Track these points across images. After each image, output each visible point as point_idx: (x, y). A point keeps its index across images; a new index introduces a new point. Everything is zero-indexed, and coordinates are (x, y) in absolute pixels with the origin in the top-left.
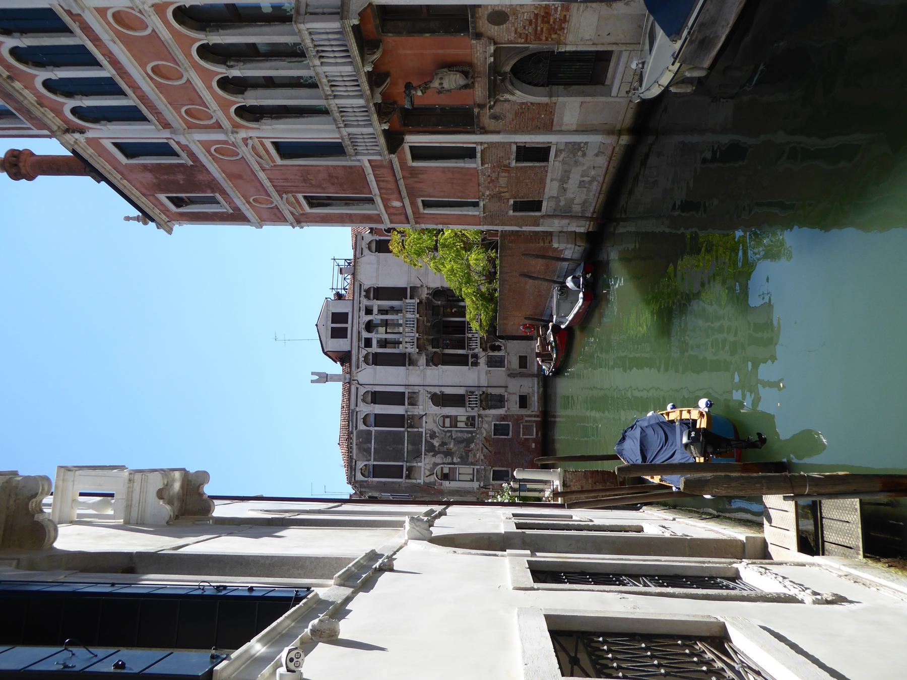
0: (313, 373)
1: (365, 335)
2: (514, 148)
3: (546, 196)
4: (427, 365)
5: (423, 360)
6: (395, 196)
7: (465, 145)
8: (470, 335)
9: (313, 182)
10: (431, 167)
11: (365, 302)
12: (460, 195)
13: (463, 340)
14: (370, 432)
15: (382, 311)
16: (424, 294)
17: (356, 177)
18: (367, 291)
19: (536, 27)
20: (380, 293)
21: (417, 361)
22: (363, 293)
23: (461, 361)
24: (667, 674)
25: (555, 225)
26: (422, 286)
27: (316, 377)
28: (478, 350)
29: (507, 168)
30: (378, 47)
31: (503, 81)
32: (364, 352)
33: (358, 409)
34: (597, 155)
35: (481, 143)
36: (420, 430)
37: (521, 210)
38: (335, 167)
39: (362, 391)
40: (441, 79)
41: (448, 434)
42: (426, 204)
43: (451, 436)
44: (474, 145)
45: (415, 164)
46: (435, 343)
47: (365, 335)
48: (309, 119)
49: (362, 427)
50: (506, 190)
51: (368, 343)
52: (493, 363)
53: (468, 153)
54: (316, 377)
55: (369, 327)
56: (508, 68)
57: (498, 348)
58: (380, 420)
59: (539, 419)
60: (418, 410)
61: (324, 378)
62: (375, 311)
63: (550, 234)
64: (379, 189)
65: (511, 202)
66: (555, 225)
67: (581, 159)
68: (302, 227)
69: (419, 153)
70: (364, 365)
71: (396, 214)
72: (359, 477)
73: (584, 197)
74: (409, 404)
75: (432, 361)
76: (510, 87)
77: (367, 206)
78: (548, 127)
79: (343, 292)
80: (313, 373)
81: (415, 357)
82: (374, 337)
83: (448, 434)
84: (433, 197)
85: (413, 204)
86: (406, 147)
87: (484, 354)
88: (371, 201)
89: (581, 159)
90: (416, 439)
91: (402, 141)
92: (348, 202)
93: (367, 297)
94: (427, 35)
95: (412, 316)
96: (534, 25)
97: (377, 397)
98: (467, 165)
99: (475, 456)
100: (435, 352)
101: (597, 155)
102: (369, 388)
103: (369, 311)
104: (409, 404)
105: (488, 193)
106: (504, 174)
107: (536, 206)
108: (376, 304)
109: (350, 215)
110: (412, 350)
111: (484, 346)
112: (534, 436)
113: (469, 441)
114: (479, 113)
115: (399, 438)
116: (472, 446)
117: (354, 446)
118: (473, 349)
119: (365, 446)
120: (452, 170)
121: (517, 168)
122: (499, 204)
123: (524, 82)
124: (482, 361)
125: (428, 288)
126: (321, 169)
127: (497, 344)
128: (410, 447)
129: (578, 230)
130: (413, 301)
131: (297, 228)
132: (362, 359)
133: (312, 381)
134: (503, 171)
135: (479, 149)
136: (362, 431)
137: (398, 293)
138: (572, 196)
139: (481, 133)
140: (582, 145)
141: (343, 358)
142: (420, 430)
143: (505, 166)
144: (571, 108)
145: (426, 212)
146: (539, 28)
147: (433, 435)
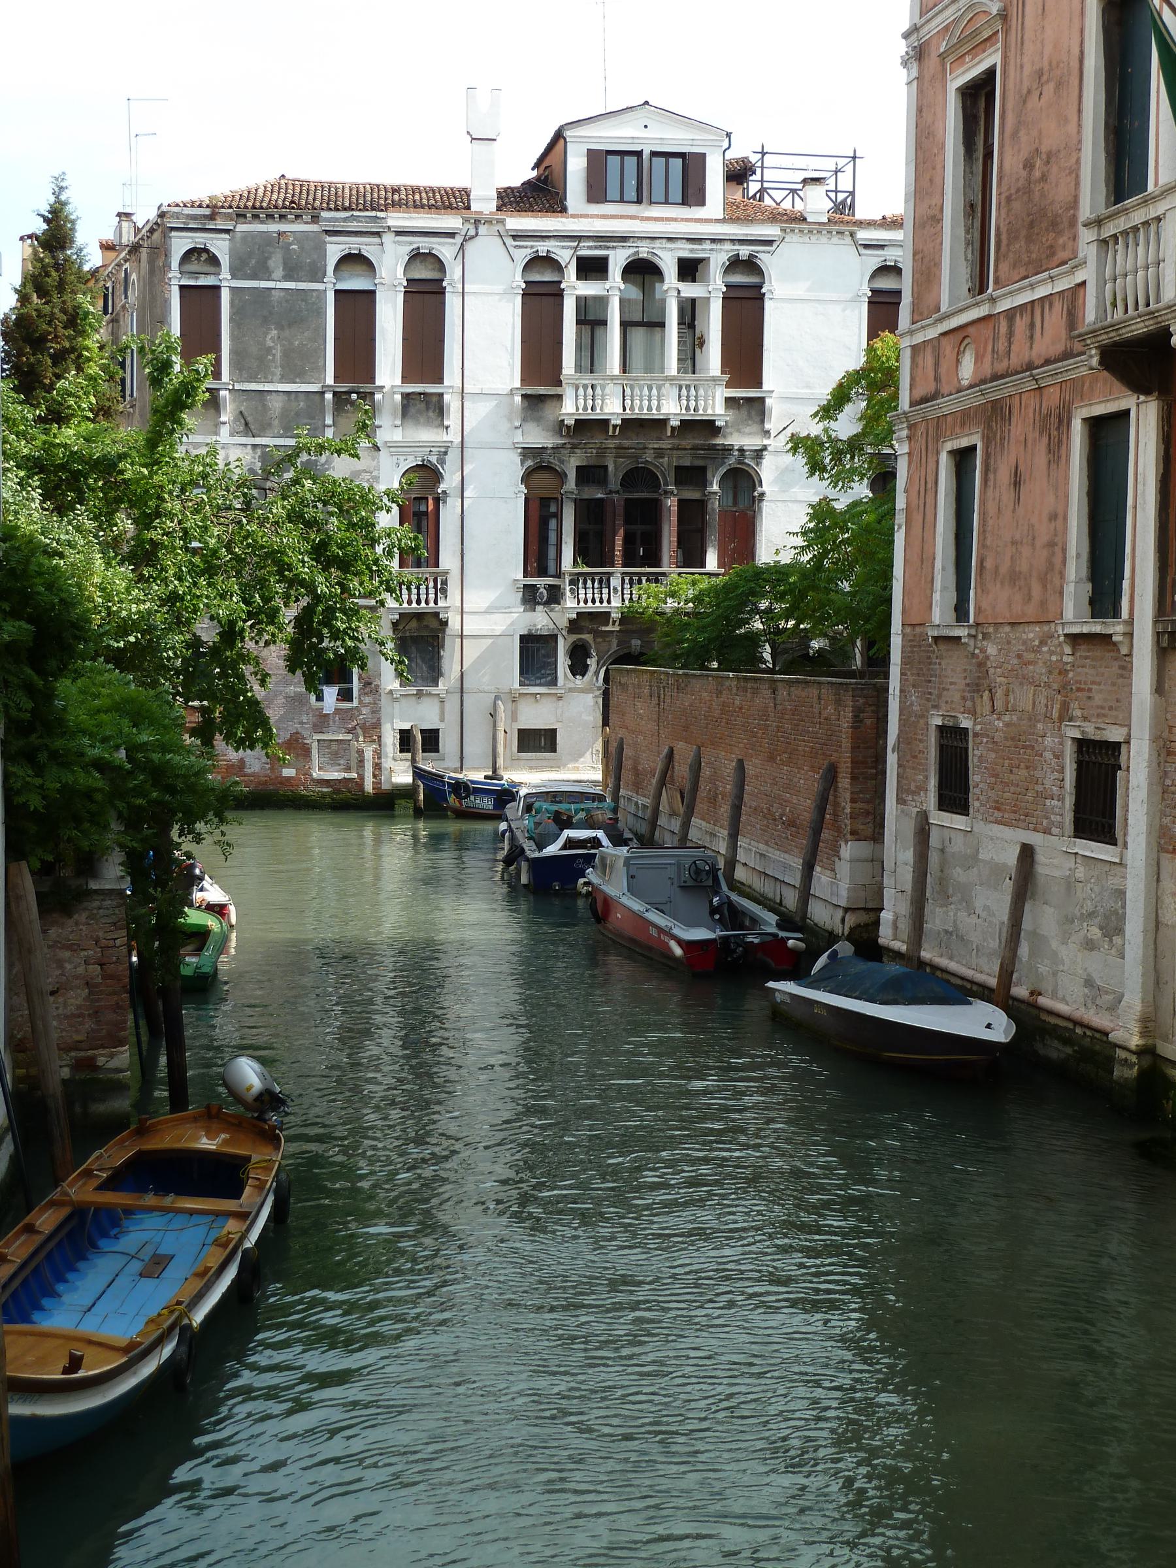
1: (618, 259)
2: (1114, 734)
3: (980, 827)
4: (527, 452)
5: (539, 437)
6: (987, 370)
7: (1126, 584)
8: (615, 582)
9: (1033, 101)
10: (1067, 478)
11: (718, 259)
12: (989, 564)
13: (605, 559)
15: (690, 312)
16: (742, 439)
17: (1043, 234)
18: (750, 265)
20: (746, 306)
21: (538, 420)
22: (744, 251)
23: (538, 553)
24: (131, 963)
25: (898, 852)
26: (767, 433)
28: (571, 604)
32: (565, 255)
33: (388, 238)
34: (1089, 983)
35: (1130, 635)
37: (942, 749)
38: (1075, 172)
39: (446, 251)
42: (962, 458)
44: (1125, 614)
45: (1077, 426)
46: (589, 474)
47: (618, 259)
49: (335, 250)
50: (999, 704)
51: (593, 268)
52: (535, 654)
53: (1105, 594)
55: (642, 271)
57: (578, 667)
58: (357, 310)
59: (369, 787)
60: (389, 430)
62: (690, 290)
63: (877, 836)
64: (1011, 314)
65: (965, 723)
66: (898, 852)
67: (1077, 938)
68: (905, 64)
69: (1107, 434)
70: (523, 255)
71: (937, 365)
72: (180, 244)
73: (975, 938)
74: (406, 396)
75: (539, 468)
77: (964, 273)
79: (753, 187)
81: (549, 412)
82: (613, 288)
84: (985, 481)
85: (966, 418)
86: (1127, 401)
87: (563, 622)
88: (980, 285)
89: (1077, 938)
91: (1140, 387)
92: (977, 210)
93: (735, 264)
95: (671, 408)
97: (426, 297)
98: (1070, 589)
100: (562, 476)
101: (1089, 983)
102: (453, 272)
103: (689, 269)
104: (406, 396)
105: (992, 650)
108: (712, 289)
109: (937, 220)
110: (570, 408)
111: (586, 623)
112: (316, 774)
117: (273, 227)
119: (276, 263)
120: (1056, 545)
122: (961, 683)
124: (540, 620)
125: (759, 454)
126: (1072, 128)
127: (592, 662)
129: (886, 916)
131: (902, 47)
132: (542, 248)
135: (1116, 629)
136: (321, 250)
137: (745, 358)
138: (979, 904)
140: (1117, 940)
141: (542, 192)
143: (1065, 706)
145: (944, 457)
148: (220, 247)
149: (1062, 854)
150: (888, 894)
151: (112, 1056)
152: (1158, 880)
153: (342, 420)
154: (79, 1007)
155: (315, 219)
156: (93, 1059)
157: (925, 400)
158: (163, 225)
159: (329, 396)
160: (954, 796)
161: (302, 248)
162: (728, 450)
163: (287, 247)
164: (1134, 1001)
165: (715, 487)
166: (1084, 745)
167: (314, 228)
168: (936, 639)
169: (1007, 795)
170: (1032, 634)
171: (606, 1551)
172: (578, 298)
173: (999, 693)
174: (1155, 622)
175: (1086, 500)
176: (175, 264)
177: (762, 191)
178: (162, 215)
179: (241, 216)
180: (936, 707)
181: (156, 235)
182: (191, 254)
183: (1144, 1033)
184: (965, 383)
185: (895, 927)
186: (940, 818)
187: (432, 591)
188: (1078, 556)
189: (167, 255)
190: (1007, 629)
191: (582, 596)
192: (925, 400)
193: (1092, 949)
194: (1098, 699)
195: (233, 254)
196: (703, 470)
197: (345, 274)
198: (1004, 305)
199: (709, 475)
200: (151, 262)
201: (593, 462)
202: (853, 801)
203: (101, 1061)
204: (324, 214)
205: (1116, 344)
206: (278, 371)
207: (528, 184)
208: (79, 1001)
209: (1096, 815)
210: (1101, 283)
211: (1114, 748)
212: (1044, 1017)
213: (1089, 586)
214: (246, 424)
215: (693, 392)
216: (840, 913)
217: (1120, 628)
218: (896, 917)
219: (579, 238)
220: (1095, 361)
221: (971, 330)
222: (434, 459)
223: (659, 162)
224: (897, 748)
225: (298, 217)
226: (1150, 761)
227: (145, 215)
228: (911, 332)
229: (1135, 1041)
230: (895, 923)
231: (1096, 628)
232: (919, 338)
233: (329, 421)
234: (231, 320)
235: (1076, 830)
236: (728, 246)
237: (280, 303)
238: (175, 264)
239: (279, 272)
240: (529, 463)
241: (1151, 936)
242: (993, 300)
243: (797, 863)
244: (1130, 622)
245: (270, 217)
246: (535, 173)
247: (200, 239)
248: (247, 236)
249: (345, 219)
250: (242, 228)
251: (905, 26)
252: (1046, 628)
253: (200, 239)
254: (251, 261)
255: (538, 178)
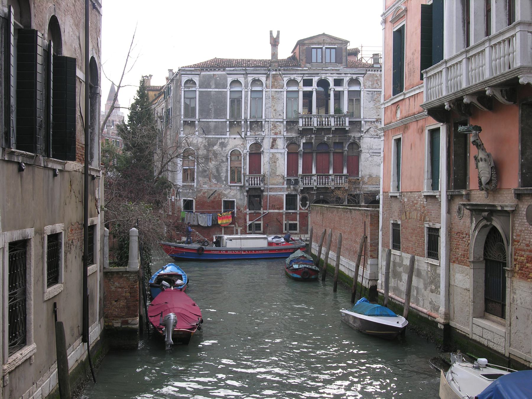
0: (278, 32)
1: (315, 79)
2: (437, 226)
4: (288, 139)
14: (225, 87)
19: (524, 251)
22: (354, 77)
27: (275, 35)
29: (423, 219)
30: (509, 100)
31: (485, 218)
35: (440, 195)
36: (228, 133)
40: (485, 160)
41: (224, 159)
42: (398, 141)
43: (223, 162)
44: (440, 190)
48: (462, 32)
49: (230, 79)
50: (408, 217)
54: (275, 35)
56: (494, 224)
61: (275, 42)
62: (338, 89)
65: (399, 222)
66: (382, 262)
68: (381, 24)
72: (184, 79)
76: (481, 225)
78: (450, 260)
80: (278, 32)
83: (224, 159)
86: (440, 125)
89: (429, 288)
90: (219, 129)
94: (520, 148)
96: (525, 248)
99: (205, 183)
100: (299, 146)
103: (338, 82)
105: (406, 200)
106: (419, 215)
107: (397, 245)
113: (218, 178)
114: (462, 195)
115: (220, 113)
116: (214, 181)
117: (212, 73)
118: (302, 181)
119: (213, 83)
121: (423, 228)
122: (398, 210)
123: (488, 237)
125: (359, 138)
128: (212, 125)
130: (347, 124)
131: (381, 19)
133: (271, 33)
134: (421, 215)
139: (447, 196)
142: (228, 133)
144: (465, 279)
146: (523, 253)
147: (223, 145)
148: (196, 79)
149: (424, 263)
150: (380, 275)
151: (133, 320)
152: (449, 271)
153: (232, 130)
154: (123, 305)
155: (224, 70)
156: (127, 321)
157: (388, 124)
158: (183, 71)
159: (228, 122)
160: (397, 245)
161: (220, 79)
162: (350, 137)
163: (216, 79)
164: (442, 309)
165: (346, 149)
166: (430, 229)
167: (224, 73)
168: (391, 196)
169: (410, 245)
170: (416, 195)
171: (7, 389)
172: (303, 92)
173: (408, 213)
174: (447, 192)
175: (430, 154)
176: (183, 85)
177: (362, 58)
178: (179, 70)
179: (202, 70)
180: (392, 217)
181: (178, 76)
182: (187, 82)
183: (445, 319)
184: (398, 119)
185: (382, 285)
186: (393, 252)
187: (258, 181)
188: (428, 171)
189: (181, 82)
190: (410, 193)
191: (305, 182)
192: (388, 124)
193: (432, 293)
194: (433, 215)
195: (200, 81)
196: (342, 143)
197: (233, 86)
198: (407, 96)
199: (344, 145)
200: (176, 84)
201: (308, 141)
202: (371, 246)
203: (130, 321)
204: (227, 69)
205: (431, 108)
206: (213, 115)
207: (289, 58)
208: (124, 304)
209: (433, 252)
210: (427, 91)
211: (438, 230)
212: (420, 314)
213: (431, 181)
214: (204, 131)
215: (338, 119)
216: (367, 281)
217: (438, 194)
218: (382, 282)
219: (304, 74)
220: (426, 113)
221: (400, 103)
222: (259, 141)
223: (328, 50)
224: (382, 230)
225: (219, 70)
226: (446, 234)
227: (175, 70)
228: (384, 104)
229: (442, 321)
230: (382, 284)
231: (432, 194)
232: (386, 105)
233: (228, 130)
234: (199, 101)
235: (428, 255)
236: (349, 75)
237: (214, 95)
238: (183, 85)
239: (213, 86)
240: (288, 142)
241: (447, 289)
242: (405, 94)
243: (354, 264)
244: (440, 192)
245: (211, 70)
246: (292, 54)
247: (190, 77)
248: (204, 76)
249: (233, 70)
250: (203, 73)
251: (382, 13)
252: (419, 193)
253: (190, 77)
254: (205, 83)
255: (292, 56)
